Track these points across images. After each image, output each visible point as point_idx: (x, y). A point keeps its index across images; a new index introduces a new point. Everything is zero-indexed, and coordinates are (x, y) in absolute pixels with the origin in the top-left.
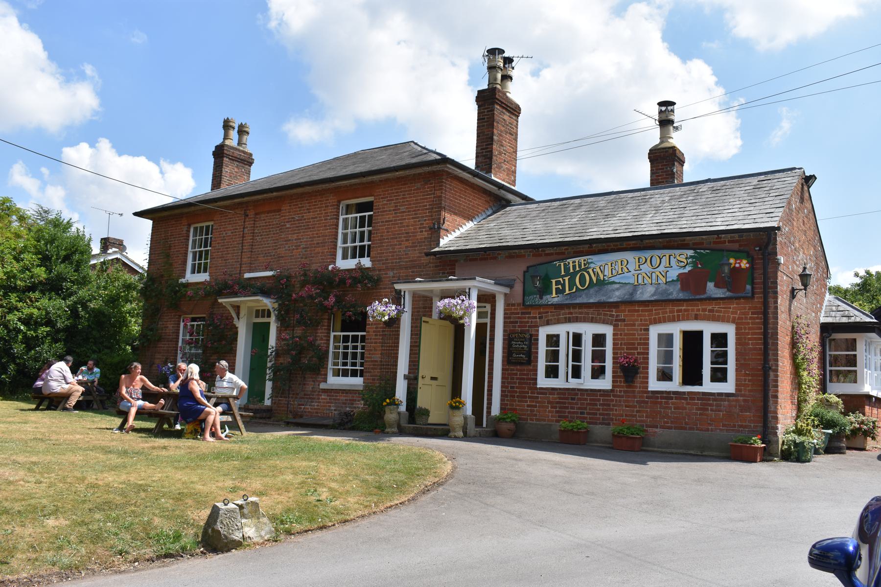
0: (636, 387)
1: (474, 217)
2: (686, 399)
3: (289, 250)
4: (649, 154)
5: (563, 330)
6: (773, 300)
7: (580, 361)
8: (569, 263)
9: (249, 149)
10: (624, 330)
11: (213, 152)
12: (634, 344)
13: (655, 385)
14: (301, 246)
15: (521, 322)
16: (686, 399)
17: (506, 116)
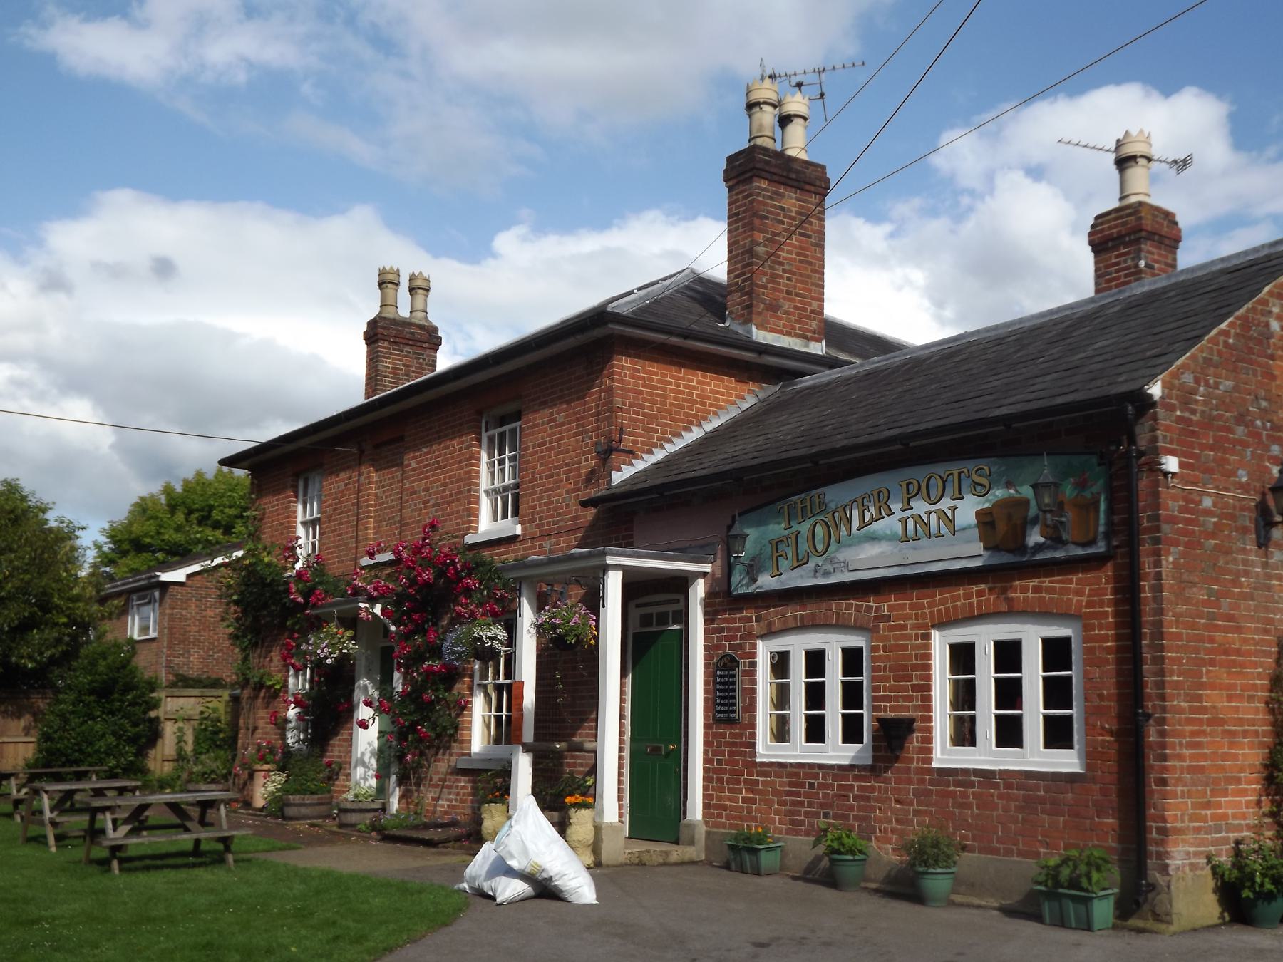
0: (911, 760)
1: (705, 419)
2: (996, 786)
3: (416, 511)
4: (1090, 234)
5: (798, 645)
6: (1151, 559)
7: (956, 683)
8: (795, 503)
9: (434, 318)
10: (887, 639)
11: (365, 333)
12: (905, 668)
13: (944, 754)
14: (431, 503)
15: (729, 629)
16: (996, 786)
17: (791, 201)
